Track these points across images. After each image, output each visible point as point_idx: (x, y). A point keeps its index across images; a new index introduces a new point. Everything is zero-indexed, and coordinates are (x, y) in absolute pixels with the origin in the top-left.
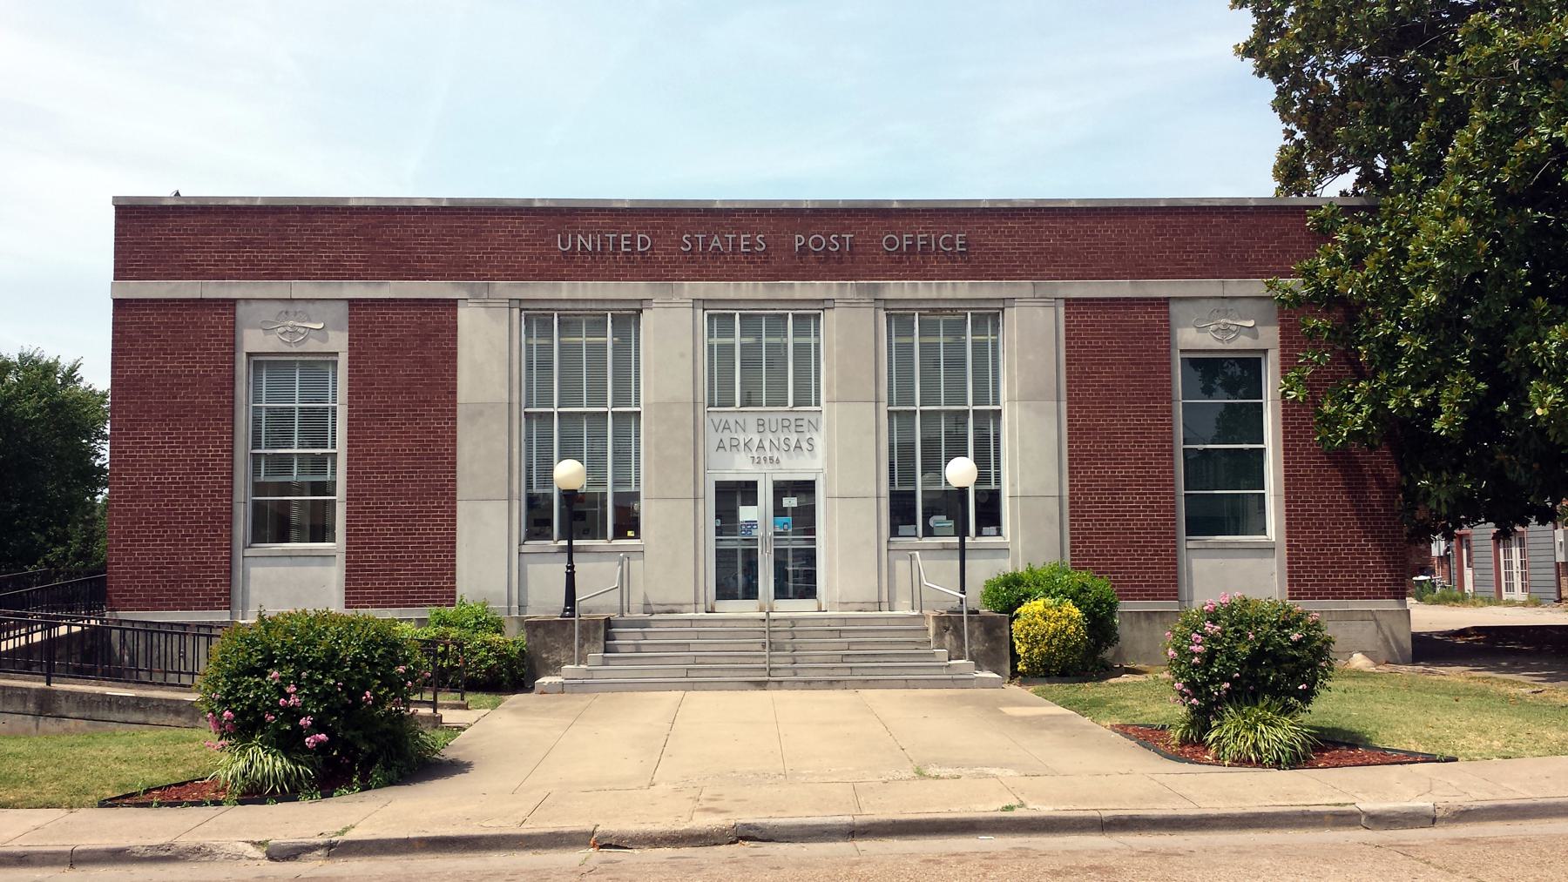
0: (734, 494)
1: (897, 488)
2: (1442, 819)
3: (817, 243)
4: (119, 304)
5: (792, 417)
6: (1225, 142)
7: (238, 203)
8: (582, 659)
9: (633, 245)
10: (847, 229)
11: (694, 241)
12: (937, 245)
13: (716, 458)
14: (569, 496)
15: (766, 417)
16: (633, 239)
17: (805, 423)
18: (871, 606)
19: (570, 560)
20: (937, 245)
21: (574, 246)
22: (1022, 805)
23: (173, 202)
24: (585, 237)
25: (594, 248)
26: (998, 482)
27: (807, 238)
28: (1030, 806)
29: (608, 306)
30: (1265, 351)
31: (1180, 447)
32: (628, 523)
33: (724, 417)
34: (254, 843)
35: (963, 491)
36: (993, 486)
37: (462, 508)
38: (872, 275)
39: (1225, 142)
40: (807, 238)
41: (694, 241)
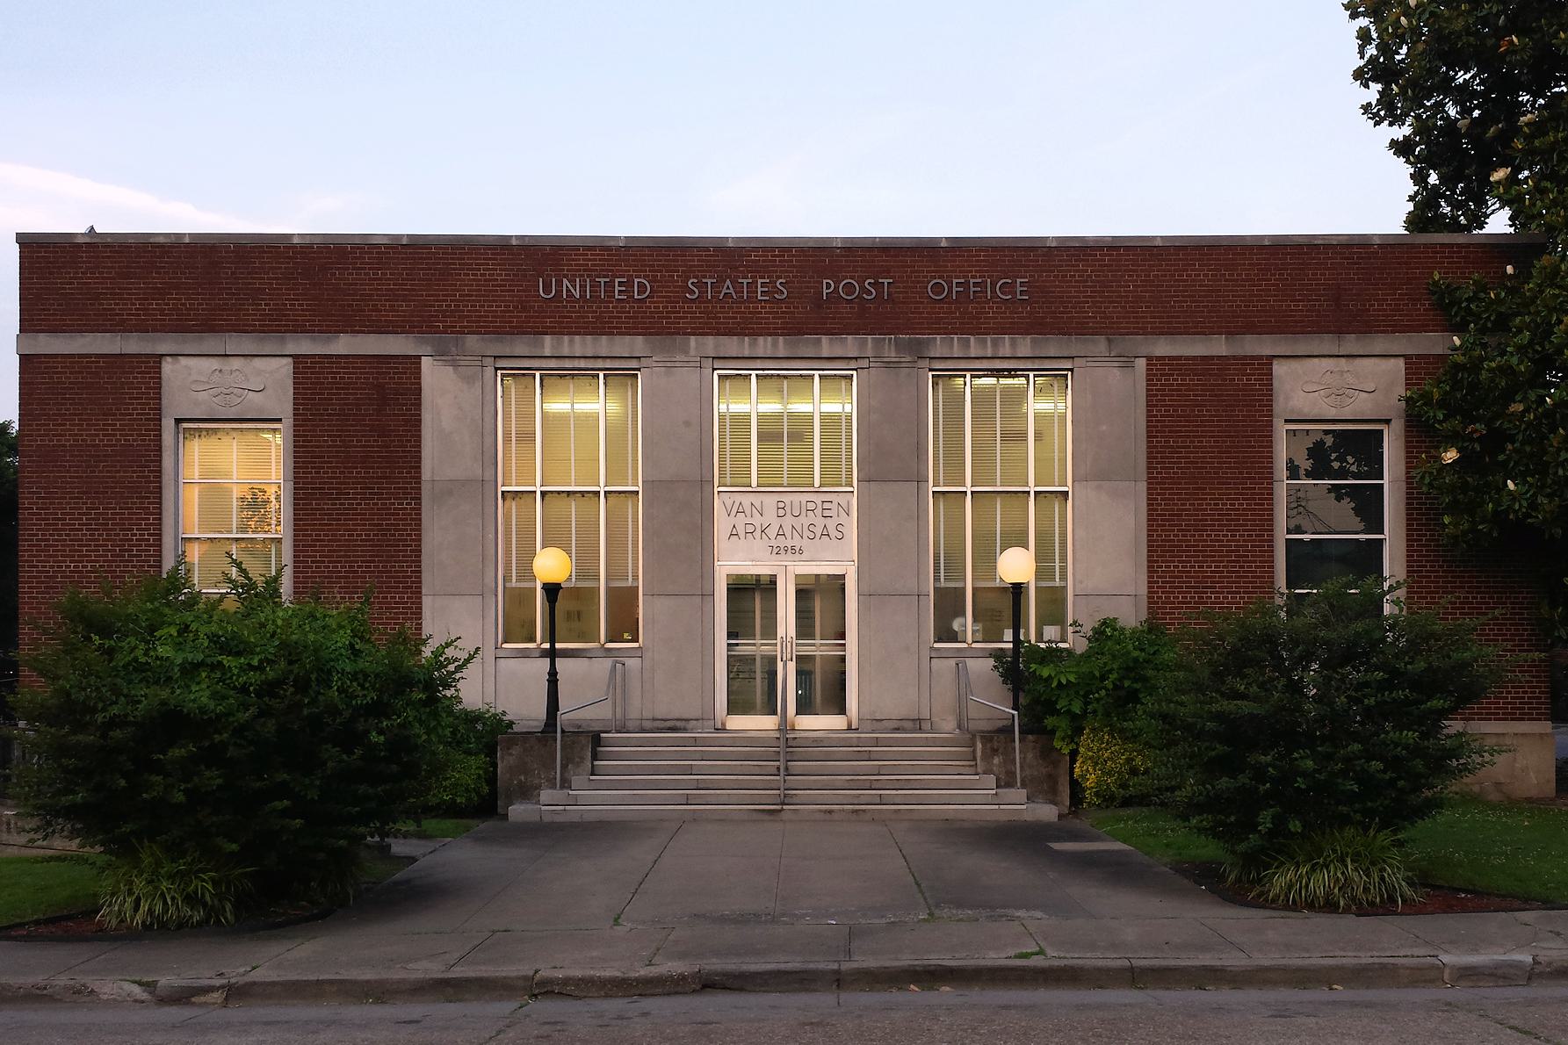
0: (750, 594)
1: (943, 584)
2: (1541, 975)
3: (849, 288)
4: (26, 361)
5: (818, 499)
6: (1358, 185)
7: (162, 240)
8: (566, 784)
9: (629, 292)
10: (886, 272)
11: (701, 286)
12: (993, 291)
13: (264, 375)
14: (552, 590)
15: (787, 499)
16: (629, 284)
17: (834, 506)
18: (908, 725)
19: (553, 664)
20: (993, 291)
21: (559, 292)
22: (1041, 952)
23: (88, 240)
24: (573, 282)
25: (583, 296)
26: (1064, 577)
27: (837, 283)
28: (1050, 952)
29: (600, 364)
30: (1388, 422)
31: (1281, 536)
32: (624, 623)
33: (738, 498)
34: (140, 983)
35: (1018, 589)
36: (1057, 583)
37: (427, 602)
38: (909, 328)
39: (1358, 185)
40: (837, 283)
41: (701, 286)
